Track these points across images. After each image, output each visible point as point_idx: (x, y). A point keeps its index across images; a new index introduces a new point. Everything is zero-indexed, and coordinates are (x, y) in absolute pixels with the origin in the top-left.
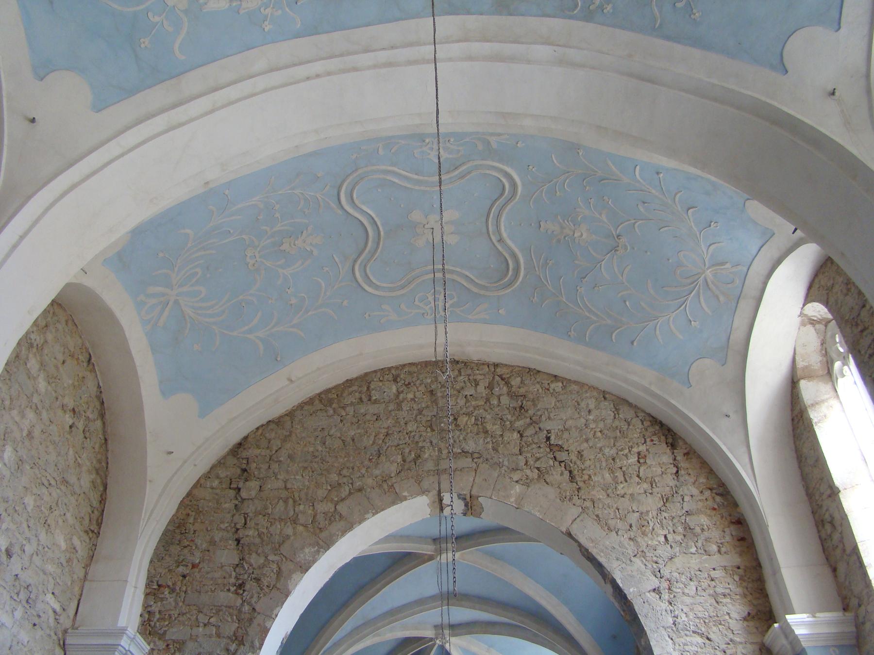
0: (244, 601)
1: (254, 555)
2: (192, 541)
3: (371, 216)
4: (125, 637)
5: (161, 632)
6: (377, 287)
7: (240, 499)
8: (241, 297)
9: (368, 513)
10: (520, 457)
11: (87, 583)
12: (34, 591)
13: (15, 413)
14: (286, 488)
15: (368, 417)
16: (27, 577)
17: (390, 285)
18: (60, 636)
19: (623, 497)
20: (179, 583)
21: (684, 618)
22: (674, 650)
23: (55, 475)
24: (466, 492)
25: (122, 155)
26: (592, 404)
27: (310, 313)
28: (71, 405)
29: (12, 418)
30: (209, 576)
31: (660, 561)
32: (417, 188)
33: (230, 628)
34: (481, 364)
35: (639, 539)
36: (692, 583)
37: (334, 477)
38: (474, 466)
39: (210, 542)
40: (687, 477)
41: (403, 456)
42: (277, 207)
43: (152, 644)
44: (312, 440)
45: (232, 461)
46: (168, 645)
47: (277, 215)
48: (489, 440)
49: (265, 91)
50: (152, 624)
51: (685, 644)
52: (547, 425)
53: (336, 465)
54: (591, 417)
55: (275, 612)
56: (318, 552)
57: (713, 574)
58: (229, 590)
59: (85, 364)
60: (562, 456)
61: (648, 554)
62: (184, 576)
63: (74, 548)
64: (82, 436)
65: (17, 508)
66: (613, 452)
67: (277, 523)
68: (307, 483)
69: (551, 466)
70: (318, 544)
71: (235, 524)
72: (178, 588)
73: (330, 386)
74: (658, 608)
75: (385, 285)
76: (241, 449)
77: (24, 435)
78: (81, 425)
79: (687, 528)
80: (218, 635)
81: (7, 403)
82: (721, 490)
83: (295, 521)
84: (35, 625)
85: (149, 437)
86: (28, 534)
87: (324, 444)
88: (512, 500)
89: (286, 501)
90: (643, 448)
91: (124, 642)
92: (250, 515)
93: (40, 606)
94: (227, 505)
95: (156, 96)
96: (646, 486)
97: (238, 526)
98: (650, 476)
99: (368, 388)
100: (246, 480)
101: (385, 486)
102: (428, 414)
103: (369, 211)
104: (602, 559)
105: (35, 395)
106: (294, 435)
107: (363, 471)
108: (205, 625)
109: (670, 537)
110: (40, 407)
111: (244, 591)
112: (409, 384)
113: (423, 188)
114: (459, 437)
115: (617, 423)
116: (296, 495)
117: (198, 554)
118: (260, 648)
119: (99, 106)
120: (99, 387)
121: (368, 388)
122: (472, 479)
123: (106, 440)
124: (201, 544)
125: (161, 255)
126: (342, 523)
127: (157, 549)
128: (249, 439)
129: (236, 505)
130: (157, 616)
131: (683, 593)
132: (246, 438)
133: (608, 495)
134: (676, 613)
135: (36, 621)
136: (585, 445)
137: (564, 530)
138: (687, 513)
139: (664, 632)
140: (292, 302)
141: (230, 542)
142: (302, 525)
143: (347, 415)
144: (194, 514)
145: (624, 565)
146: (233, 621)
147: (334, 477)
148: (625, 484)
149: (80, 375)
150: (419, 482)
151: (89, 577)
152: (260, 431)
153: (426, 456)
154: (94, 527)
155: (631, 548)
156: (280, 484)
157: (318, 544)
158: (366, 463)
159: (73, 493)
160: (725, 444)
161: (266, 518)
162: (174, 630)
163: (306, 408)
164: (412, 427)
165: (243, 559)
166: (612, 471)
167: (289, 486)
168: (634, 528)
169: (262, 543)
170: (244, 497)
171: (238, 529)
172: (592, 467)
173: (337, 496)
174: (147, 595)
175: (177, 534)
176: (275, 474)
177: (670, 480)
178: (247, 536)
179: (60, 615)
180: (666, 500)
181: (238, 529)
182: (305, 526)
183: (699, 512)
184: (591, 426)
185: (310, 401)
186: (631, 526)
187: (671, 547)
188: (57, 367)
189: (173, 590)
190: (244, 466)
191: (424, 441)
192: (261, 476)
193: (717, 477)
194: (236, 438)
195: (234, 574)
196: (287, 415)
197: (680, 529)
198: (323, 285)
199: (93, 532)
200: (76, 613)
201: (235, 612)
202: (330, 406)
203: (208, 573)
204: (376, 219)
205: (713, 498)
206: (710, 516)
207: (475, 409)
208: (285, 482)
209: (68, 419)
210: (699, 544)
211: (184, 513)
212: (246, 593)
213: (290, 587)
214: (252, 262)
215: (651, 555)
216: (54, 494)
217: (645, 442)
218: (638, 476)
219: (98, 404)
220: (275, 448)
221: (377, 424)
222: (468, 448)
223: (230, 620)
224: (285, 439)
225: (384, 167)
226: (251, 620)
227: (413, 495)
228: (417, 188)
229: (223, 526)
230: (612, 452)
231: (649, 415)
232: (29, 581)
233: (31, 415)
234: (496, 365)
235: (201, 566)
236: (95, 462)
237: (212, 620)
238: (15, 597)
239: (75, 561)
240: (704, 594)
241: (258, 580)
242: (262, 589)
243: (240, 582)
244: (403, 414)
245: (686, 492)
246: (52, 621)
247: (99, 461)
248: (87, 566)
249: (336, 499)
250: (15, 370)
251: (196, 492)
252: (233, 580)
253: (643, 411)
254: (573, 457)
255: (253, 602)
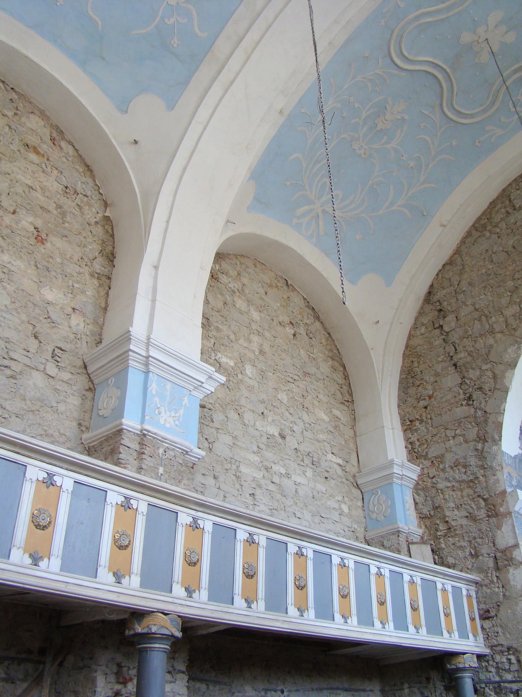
0: (476, 409)
1: (471, 371)
2: (422, 379)
3: (432, 63)
4: (395, 466)
5: (424, 454)
6: (472, 116)
7: (445, 334)
8: (370, 183)
11: (357, 438)
12: (315, 456)
13: (241, 341)
14: (476, 310)
16: (305, 448)
17: (482, 108)
18: (352, 480)
20: (424, 414)
23: (296, 372)
25: (205, 128)
27: (430, 166)
28: (287, 320)
29: (241, 345)
30: (444, 400)
32: (451, 14)
33: (472, 433)
37: (510, 284)
39: (435, 375)
42: (352, 99)
43: (421, 465)
44: (481, 263)
46: (432, 462)
47: (357, 105)
49: (276, 17)
50: (416, 450)
53: (508, 273)
55: (502, 408)
58: (462, 405)
59: (285, 288)
62: (426, 408)
63: (337, 418)
64: (307, 338)
65: (275, 404)
67: (480, 339)
68: (491, 298)
70: (517, 342)
71: (448, 354)
72: (424, 418)
73: (479, 214)
75: (478, 110)
76: (432, 296)
77: (257, 353)
78: (302, 330)
80: (466, 442)
81: (232, 337)
83: (492, 332)
84: (326, 478)
85: (357, 319)
86: (291, 418)
87: (492, 261)
89: (480, 320)
91: (396, 470)
92: (457, 342)
93: (324, 464)
94: (437, 342)
95: (205, 72)
97: (451, 354)
99: (510, 200)
100: (444, 317)
103: (426, 59)
105: (253, 324)
106: (466, 266)
108: (454, 437)
110: (261, 331)
111: (473, 401)
113: (456, 11)
116: (486, 312)
117: (429, 387)
118: (500, 440)
119: (171, 106)
120: (305, 299)
121: (510, 200)
123: (329, 334)
124: (429, 379)
125: (288, 184)
127: (399, 395)
128: (435, 286)
129: (444, 340)
130: (417, 443)
132: (432, 286)
135: (327, 475)
140: (411, 165)
141: (450, 369)
142: (499, 332)
143: (501, 230)
144: (416, 359)
146: (473, 427)
147: (510, 284)
149: (285, 297)
151: (358, 434)
152: (440, 275)
154: (347, 397)
156: (471, 308)
157: (517, 342)
159: (318, 380)
161: (470, 339)
162: (433, 449)
165: (464, 377)
167: (477, 307)
169: (473, 359)
170: (447, 331)
171: (452, 357)
173: (518, 298)
174: (405, 431)
175: (409, 379)
176: (464, 303)
179: (345, 467)
181: (452, 357)
182: (502, 332)
185: (469, 234)
188: (262, 299)
189: (421, 421)
190: (439, 308)
192: (454, 309)
194: (425, 289)
195: (461, 391)
198: (427, 138)
199: (348, 401)
200: (359, 462)
201: (472, 420)
202: (486, 230)
203: (442, 398)
204: (436, 61)
208: (474, 305)
209: (290, 331)
211: (409, 361)
212: (475, 402)
213: (507, 384)
214: (362, 152)
216: (301, 385)
219: (310, 312)
220: (456, 283)
223: (470, 427)
224: (461, 272)
225: (411, 16)
226: (486, 421)
228: (451, 14)
229: (440, 359)
232: (308, 450)
233: (255, 338)
235: (435, 395)
236: (327, 352)
237: (457, 432)
238: (302, 463)
239: (342, 427)
241: (480, 389)
243: (468, 395)
246: (339, 471)
247: (331, 350)
248: (353, 427)
249: (518, 300)
250: (228, 313)
251: (411, 342)
252: (462, 396)
255: (483, 407)
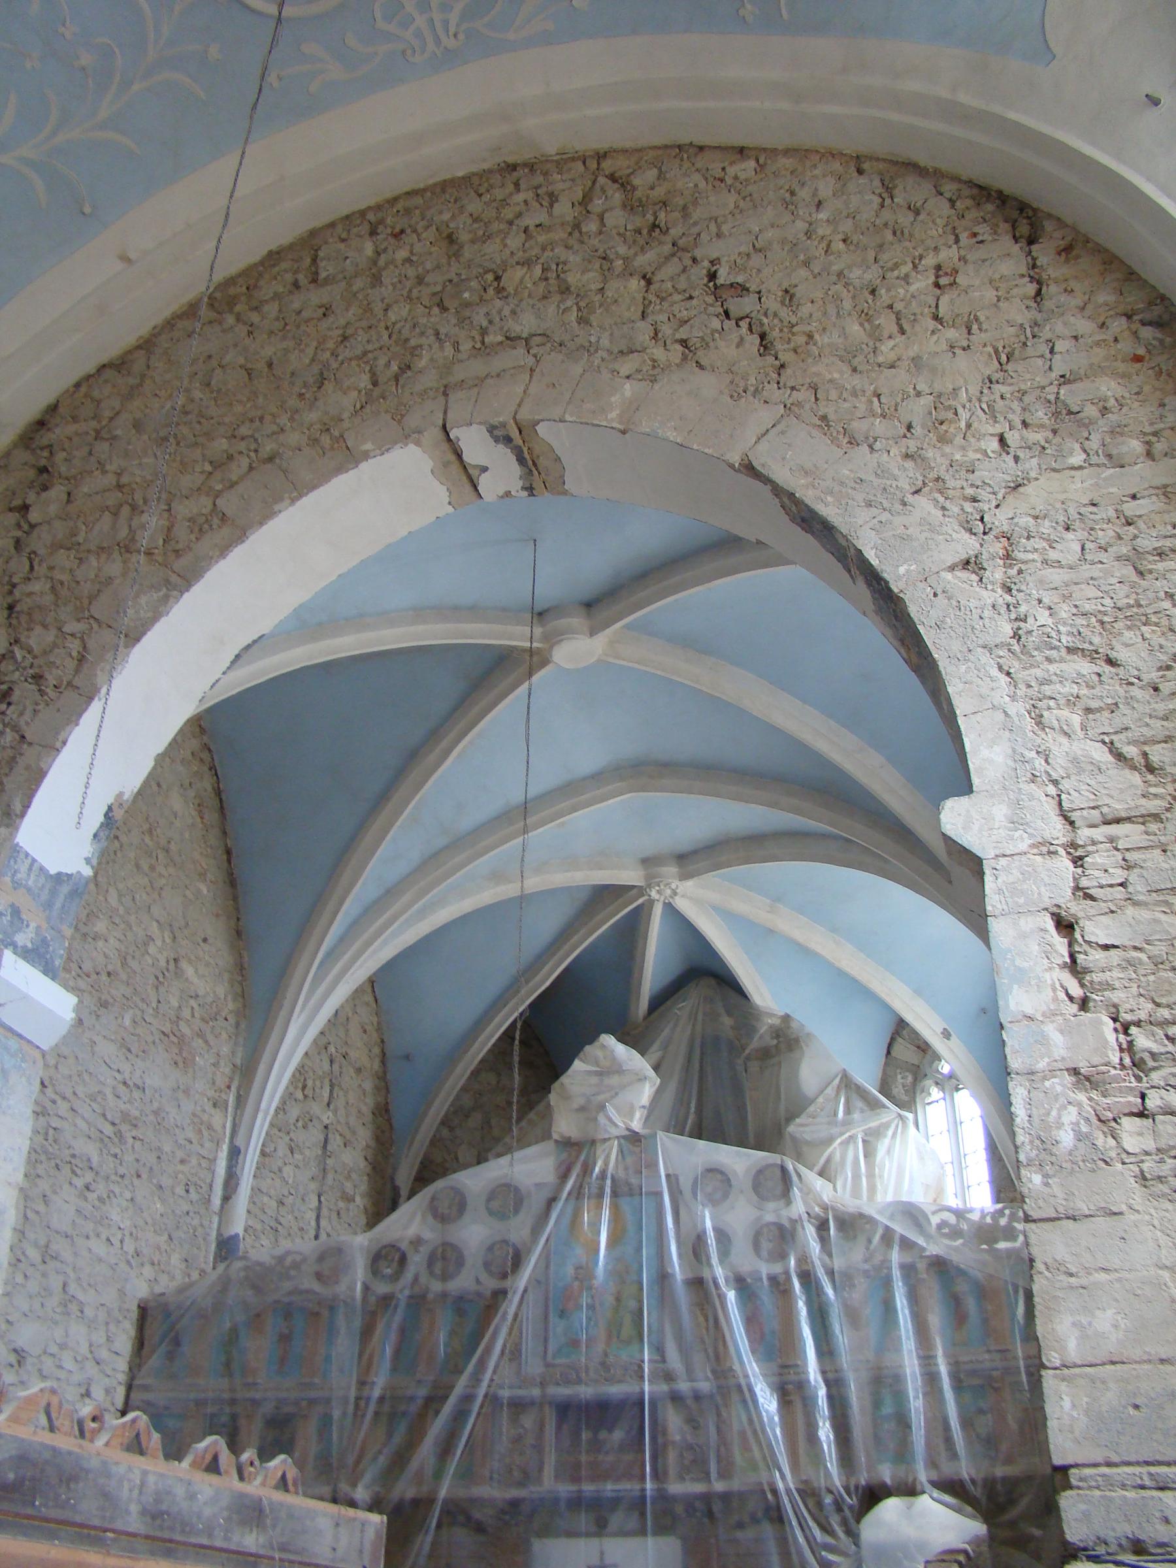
1: (38, 629)
7: (26, 527)
9: (281, 499)
10: (641, 325)
15: (306, 314)
19: (892, 367)
21: (1044, 617)
22: (1013, 698)
24: (505, 417)
26: (826, 188)
31: (983, 494)
34: (563, 161)
35: (930, 454)
36: (1070, 535)
37: (221, 444)
38: (530, 361)
40: (1063, 298)
41: (373, 374)
45: (22, 456)
48: (569, 303)
51: (1044, 682)
52: (709, 250)
54: (822, 216)
56: (166, 598)
57: (1130, 508)
60: (747, 305)
61: (951, 483)
66: (872, 275)
69: (714, 331)
74: (973, 604)
79: (1062, 413)
82: (1157, 310)
87: (208, 385)
88: (613, 415)
90: (948, 255)
96: (951, 334)
97: (15, 580)
98: (967, 310)
99: (314, 260)
101: (326, 440)
102: (436, 280)
104: (829, 511)
107: (284, 420)
109: (1012, 438)
111: (9, 704)
112: (402, 232)
114: (500, 312)
115: (886, 215)
118: (23, 815)
122: (519, 390)
126: (226, 531)
131: (1045, 562)
133: (855, 370)
134: (1023, 609)
136: (803, 272)
137: (736, 459)
138: (1064, 380)
139: (985, 658)
145: (885, 516)
148: (900, 339)
150: (399, 417)
152: (83, 389)
153: (422, 363)
155: (905, 476)
157: (167, 582)
158: (293, 402)
160: (1149, 179)
163: (180, 324)
164: (399, 312)
166: (866, 317)
168: (918, 430)
172: (817, 315)
177: (1018, 312)
178: (30, 594)
180: (1005, 358)
181: (14, 586)
183: (1095, 371)
184: (820, 232)
186: (909, 427)
187: (1016, 459)
190: (43, 462)
191: (422, 334)
193: (1143, 283)
196: (139, 347)
197: (1041, 415)
205: (1135, 333)
206: (1123, 376)
207: (544, 249)
210: (1094, 444)
215: (958, 484)
217: (957, 241)
218: (936, 318)
220: (107, 414)
221: (325, 324)
222: (518, 328)
224: (130, 395)
227: (384, 447)
230: (868, 276)
231: (970, 183)
234: (601, 156)
240: (1102, 556)
242: (42, 693)
244: (386, 291)
245: (1059, 328)
253: (956, 179)
254: (771, 303)
255: (22, 723)
